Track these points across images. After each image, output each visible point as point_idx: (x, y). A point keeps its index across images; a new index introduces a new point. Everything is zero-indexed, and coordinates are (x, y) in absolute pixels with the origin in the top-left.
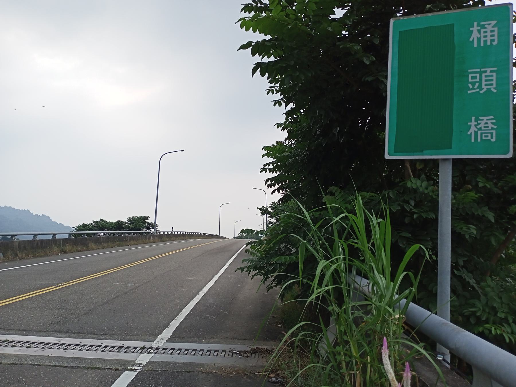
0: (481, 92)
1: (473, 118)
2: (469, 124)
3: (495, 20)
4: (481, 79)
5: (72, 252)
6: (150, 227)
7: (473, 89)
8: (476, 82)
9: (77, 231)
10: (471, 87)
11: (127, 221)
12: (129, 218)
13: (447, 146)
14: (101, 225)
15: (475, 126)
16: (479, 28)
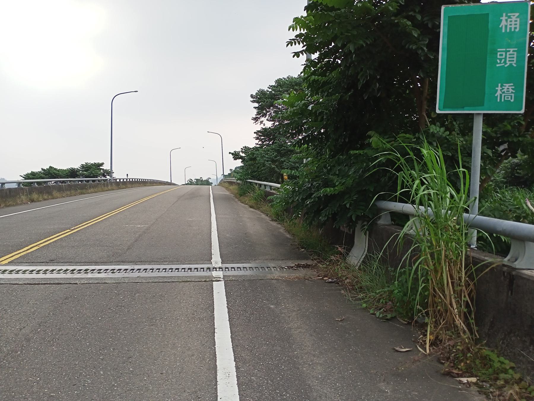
0: (506, 66)
1: (500, 85)
2: (496, 88)
3: (518, 13)
4: (506, 57)
5: (40, 201)
6: (106, 174)
7: (500, 63)
8: (502, 58)
9: (26, 179)
10: (499, 61)
11: (80, 168)
12: (82, 165)
13: (480, 104)
14: (51, 173)
15: (501, 90)
16: (507, 18)
